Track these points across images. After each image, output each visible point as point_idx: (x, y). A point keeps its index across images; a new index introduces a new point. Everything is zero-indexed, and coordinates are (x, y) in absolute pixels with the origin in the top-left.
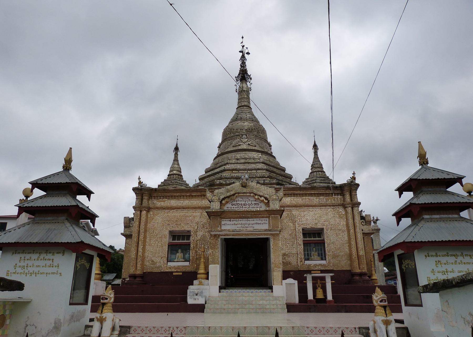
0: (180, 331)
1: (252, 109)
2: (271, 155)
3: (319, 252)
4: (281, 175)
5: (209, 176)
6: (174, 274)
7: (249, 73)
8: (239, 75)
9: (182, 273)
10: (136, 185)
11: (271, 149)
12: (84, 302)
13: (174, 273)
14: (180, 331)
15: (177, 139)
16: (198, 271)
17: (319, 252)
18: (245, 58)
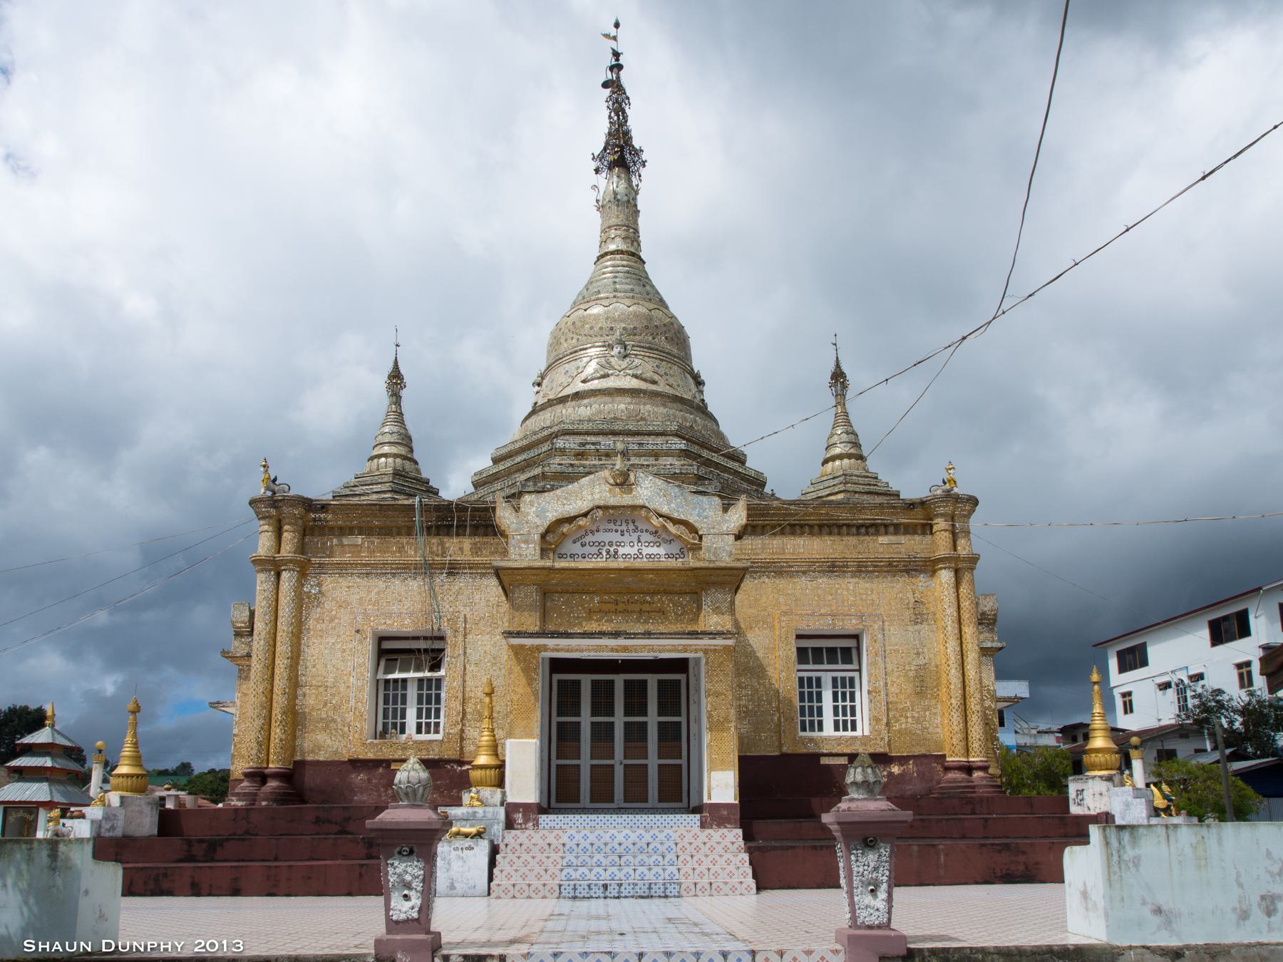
0: (713, 875)
1: (644, 263)
2: (702, 409)
3: (819, 704)
4: (736, 473)
5: (509, 473)
6: (824, 761)
7: (636, 143)
8: (605, 149)
9: (846, 758)
10: (261, 491)
11: (702, 392)
12: (735, 800)
13: (392, 764)
14: (713, 875)
15: (397, 345)
16: (475, 758)
17: (819, 704)
18: (625, 93)
